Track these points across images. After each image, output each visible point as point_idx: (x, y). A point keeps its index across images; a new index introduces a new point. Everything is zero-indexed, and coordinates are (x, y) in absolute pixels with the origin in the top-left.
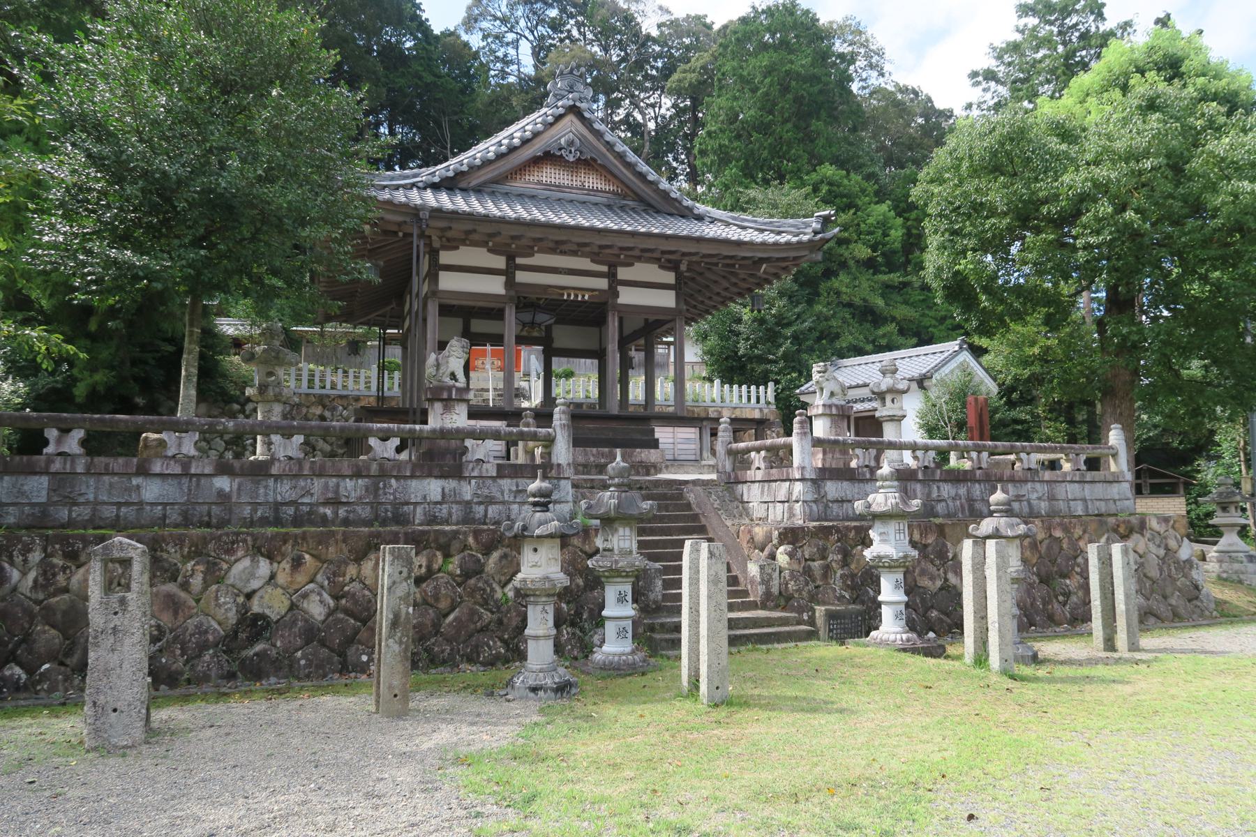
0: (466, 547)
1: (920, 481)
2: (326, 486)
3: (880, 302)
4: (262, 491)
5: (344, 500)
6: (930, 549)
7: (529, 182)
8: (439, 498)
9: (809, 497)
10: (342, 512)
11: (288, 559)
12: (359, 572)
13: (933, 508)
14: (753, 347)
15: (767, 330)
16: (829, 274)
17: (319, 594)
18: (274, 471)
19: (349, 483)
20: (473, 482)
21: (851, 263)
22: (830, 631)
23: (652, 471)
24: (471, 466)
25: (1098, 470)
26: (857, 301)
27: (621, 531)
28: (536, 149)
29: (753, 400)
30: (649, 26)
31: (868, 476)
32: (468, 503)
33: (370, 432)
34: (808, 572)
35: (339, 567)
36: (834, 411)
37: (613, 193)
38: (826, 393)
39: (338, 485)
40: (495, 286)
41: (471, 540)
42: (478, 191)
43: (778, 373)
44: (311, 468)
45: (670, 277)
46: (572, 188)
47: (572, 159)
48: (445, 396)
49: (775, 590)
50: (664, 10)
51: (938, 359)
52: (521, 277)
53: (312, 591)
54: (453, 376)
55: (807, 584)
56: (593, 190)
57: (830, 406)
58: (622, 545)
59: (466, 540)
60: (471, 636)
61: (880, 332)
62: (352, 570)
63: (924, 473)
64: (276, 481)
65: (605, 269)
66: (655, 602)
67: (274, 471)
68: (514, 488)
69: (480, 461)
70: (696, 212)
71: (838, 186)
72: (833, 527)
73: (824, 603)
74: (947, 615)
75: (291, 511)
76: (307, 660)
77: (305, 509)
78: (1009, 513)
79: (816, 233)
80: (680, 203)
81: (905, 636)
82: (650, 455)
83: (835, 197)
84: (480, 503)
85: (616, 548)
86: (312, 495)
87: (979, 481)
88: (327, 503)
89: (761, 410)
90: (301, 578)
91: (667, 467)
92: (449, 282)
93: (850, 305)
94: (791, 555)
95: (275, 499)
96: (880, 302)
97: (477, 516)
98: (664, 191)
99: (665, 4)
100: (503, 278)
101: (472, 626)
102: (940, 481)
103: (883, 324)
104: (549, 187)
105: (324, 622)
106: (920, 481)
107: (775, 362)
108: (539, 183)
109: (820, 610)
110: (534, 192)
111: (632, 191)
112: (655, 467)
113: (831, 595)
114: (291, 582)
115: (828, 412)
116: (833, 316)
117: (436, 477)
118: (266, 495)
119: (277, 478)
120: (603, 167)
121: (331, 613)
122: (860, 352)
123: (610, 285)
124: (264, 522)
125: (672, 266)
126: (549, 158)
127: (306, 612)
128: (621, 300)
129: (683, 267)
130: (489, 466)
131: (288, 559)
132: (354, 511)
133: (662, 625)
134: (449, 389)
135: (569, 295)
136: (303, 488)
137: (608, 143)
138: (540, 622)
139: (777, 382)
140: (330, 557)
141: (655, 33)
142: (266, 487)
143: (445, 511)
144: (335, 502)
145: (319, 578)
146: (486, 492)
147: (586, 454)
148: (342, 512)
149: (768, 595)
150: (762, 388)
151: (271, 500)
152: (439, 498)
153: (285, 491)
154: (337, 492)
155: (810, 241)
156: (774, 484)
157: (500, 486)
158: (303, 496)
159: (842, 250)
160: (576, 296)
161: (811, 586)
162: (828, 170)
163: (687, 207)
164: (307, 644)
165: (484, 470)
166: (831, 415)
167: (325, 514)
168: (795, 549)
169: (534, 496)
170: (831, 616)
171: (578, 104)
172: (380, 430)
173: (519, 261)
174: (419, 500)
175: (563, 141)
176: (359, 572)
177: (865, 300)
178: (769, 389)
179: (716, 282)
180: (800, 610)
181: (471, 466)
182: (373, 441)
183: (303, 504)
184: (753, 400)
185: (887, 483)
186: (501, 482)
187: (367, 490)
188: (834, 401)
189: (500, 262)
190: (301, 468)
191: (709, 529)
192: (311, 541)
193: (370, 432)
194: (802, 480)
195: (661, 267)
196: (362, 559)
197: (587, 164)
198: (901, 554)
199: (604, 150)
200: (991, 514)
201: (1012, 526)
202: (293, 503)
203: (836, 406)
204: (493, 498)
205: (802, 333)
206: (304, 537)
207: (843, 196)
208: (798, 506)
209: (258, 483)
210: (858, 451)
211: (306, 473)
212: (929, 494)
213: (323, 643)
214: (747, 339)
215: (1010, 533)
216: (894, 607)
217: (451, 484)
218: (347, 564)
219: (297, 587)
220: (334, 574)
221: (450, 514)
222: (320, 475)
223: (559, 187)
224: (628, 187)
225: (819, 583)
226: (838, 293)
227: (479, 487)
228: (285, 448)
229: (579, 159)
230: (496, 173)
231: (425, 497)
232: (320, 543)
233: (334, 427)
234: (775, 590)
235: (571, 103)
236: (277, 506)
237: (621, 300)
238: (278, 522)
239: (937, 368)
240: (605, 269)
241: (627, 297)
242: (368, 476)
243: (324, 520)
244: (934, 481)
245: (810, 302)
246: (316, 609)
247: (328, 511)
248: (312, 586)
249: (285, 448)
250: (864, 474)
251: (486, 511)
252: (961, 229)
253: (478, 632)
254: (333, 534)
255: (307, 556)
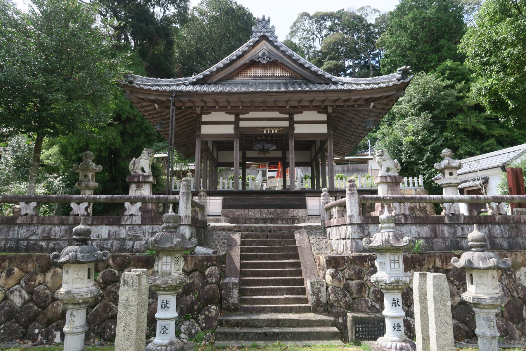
0: (108, 266)
1: (447, 224)
2: (44, 230)
3: (484, 128)
4: (11, 232)
5: (53, 237)
6: (451, 273)
7: (245, 77)
8: (106, 237)
9: (356, 236)
10: (51, 245)
11: (6, 271)
12: (44, 280)
13: (458, 243)
14: (410, 157)
15: (417, 147)
16: (451, 115)
17: (20, 291)
18: (18, 222)
19: (57, 228)
20: (127, 227)
21: (465, 108)
22: (356, 332)
23: (296, 221)
24: (126, 218)
25: (233, 163)
26: (469, 127)
27: (164, 259)
28: (246, 59)
29: (411, 184)
30: (371, 20)
31: (403, 221)
32: (124, 239)
33: (72, 200)
34: (347, 287)
35: (32, 276)
36: (389, 180)
37: (290, 77)
38: (384, 169)
39: (51, 229)
40: (229, 130)
41: (111, 262)
42: (216, 83)
43: (424, 170)
44: (37, 220)
45: (324, 117)
46: (267, 77)
47: (264, 62)
48: (136, 180)
49: (323, 299)
50: (376, 11)
51: (515, 154)
52: (242, 124)
53: (16, 289)
54: (143, 170)
55: (345, 296)
56: (279, 76)
57: (386, 177)
58: (164, 268)
59: (108, 262)
60: (104, 321)
61: (485, 144)
62: (40, 278)
63: (450, 218)
64: (19, 227)
65: (287, 116)
66: (234, 304)
67: (18, 222)
68: (150, 231)
69: (132, 215)
70: (333, 80)
71: (455, 70)
72: (366, 257)
73: (353, 311)
74: (465, 323)
75: (25, 243)
76: (5, 330)
77: (32, 242)
78: (483, 248)
79: (399, 80)
80: (324, 76)
81: (399, 345)
82: (300, 212)
83: (454, 76)
84: (130, 240)
85: (160, 270)
86: (37, 234)
87: (499, 224)
88: (43, 239)
89: (415, 190)
90: (11, 282)
91: (309, 219)
92: (206, 130)
93: (465, 130)
94: (333, 276)
95: (18, 237)
96: (484, 128)
97: (128, 247)
98: (314, 71)
99: (376, 8)
100: (233, 126)
101: (105, 315)
102: (464, 224)
103: (487, 140)
104: (255, 77)
105: (21, 307)
106: (447, 224)
107: (423, 164)
108: (251, 76)
109: (350, 315)
110: (247, 81)
111: (301, 76)
112: (298, 219)
113: (364, 305)
114: (6, 284)
115: (384, 180)
116: (455, 137)
117: (106, 225)
118: (13, 234)
119: (21, 225)
120: (282, 64)
121: (25, 303)
122: (472, 155)
123: (290, 124)
124: (11, 249)
125: (322, 110)
126: (253, 64)
127: (12, 302)
128: (295, 132)
129: (330, 110)
130: (136, 218)
131: (6, 271)
132: (58, 244)
133: (227, 321)
134: (138, 177)
135: (267, 131)
136: (32, 231)
137: (282, 51)
138: (75, 321)
139: (424, 175)
140: (29, 270)
141: (373, 22)
142: (14, 230)
143: (109, 244)
144: (48, 239)
145: (22, 282)
146: (133, 233)
147: (261, 213)
148: (51, 245)
149: (318, 302)
150: (416, 178)
151: (15, 237)
152: (106, 237)
153: (23, 232)
154: (49, 233)
155: (394, 85)
156: (340, 227)
157: (143, 230)
158: (31, 235)
159: (460, 103)
160: (271, 131)
161: (348, 298)
162: (449, 63)
163: (328, 78)
164: (8, 320)
165: (134, 220)
166: (387, 183)
167: (42, 246)
168: (337, 272)
169: (472, 241)
170: (356, 321)
171: (266, 34)
172: (77, 198)
173: (241, 116)
174: (95, 238)
175: (260, 54)
176: (44, 280)
177: (473, 127)
178: (420, 179)
179: (353, 118)
180: (337, 315)
181: (126, 218)
182: (73, 205)
183: (31, 240)
184: (411, 184)
185: (385, 225)
186: (144, 227)
187: (66, 232)
188: (390, 173)
189: (232, 118)
190: (32, 220)
191: (300, 258)
192: (17, 261)
193: (72, 200)
194: (351, 224)
195: (318, 112)
196: (46, 272)
197: (273, 64)
198: (393, 280)
199: (281, 55)
200: (469, 249)
201: (484, 259)
202: (26, 239)
203: (390, 177)
204: (138, 236)
205: (437, 147)
206: (15, 258)
207: (458, 75)
208: (349, 241)
209: (10, 228)
210: (396, 205)
211: (35, 222)
212: (455, 233)
213: (17, 321)
214: (406, 154)
215: (481, 265)
216: (392, 320)
217: (114, 228)
218: (37, 274)
219: (9, 286)
220: (29, 280)
221: (112, 246)
222: (42, 224)
223: (260, 77)
224: (297, 73)
225: (355, 296)
226: (457, 125)
227: (129, 231)
228: (26, 209)
229: (269, 62)
230: (226, 74)
231: (98, 236)
232: (22, 262)
233: (52, 197)
234: (323, 299)
235: (262, 34)
236: (18, 240)
237: (295, 132)
238: (17, 249)
239: (512, 160)
240: (287, 116)
241: (299, 129)
242: (67, 224)
243: (42, 249)
244: (459, 224)
245: (441, 132)
246: (17, 300)
247: (44, 244)
248: (18, 286)
249: (26, 209)
250: (400, 220)
251: (133, 244)
252: (488, 61)
253: (109, 319)
254: (30, 257)
255: (16, 269)
